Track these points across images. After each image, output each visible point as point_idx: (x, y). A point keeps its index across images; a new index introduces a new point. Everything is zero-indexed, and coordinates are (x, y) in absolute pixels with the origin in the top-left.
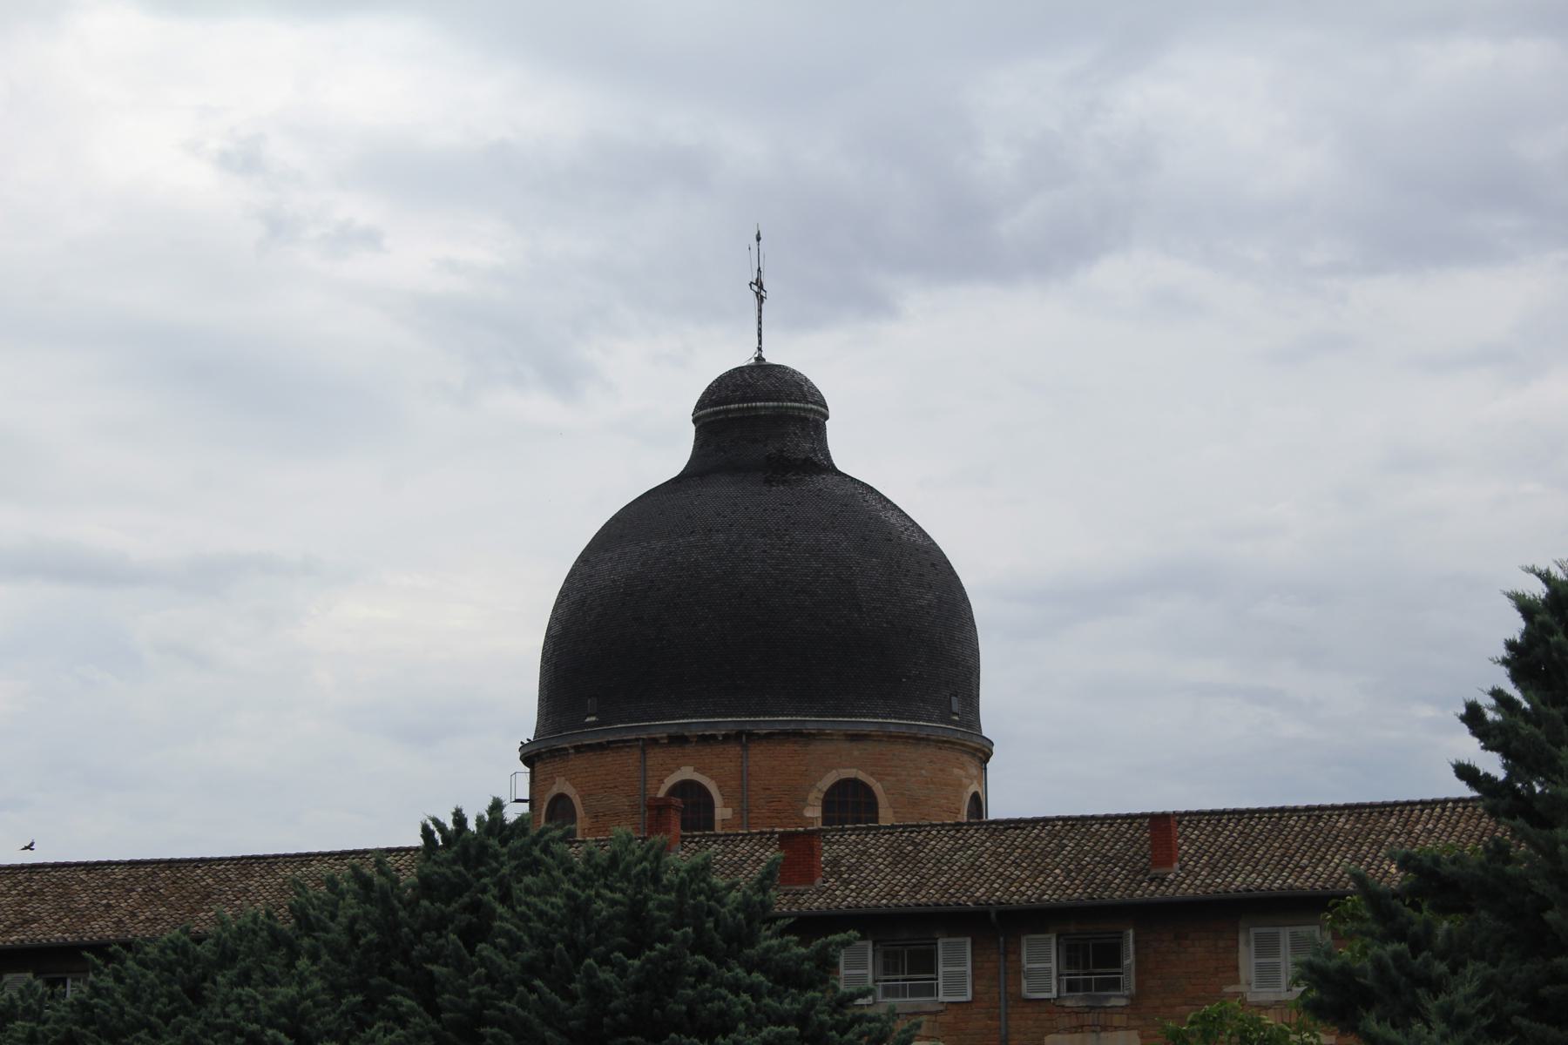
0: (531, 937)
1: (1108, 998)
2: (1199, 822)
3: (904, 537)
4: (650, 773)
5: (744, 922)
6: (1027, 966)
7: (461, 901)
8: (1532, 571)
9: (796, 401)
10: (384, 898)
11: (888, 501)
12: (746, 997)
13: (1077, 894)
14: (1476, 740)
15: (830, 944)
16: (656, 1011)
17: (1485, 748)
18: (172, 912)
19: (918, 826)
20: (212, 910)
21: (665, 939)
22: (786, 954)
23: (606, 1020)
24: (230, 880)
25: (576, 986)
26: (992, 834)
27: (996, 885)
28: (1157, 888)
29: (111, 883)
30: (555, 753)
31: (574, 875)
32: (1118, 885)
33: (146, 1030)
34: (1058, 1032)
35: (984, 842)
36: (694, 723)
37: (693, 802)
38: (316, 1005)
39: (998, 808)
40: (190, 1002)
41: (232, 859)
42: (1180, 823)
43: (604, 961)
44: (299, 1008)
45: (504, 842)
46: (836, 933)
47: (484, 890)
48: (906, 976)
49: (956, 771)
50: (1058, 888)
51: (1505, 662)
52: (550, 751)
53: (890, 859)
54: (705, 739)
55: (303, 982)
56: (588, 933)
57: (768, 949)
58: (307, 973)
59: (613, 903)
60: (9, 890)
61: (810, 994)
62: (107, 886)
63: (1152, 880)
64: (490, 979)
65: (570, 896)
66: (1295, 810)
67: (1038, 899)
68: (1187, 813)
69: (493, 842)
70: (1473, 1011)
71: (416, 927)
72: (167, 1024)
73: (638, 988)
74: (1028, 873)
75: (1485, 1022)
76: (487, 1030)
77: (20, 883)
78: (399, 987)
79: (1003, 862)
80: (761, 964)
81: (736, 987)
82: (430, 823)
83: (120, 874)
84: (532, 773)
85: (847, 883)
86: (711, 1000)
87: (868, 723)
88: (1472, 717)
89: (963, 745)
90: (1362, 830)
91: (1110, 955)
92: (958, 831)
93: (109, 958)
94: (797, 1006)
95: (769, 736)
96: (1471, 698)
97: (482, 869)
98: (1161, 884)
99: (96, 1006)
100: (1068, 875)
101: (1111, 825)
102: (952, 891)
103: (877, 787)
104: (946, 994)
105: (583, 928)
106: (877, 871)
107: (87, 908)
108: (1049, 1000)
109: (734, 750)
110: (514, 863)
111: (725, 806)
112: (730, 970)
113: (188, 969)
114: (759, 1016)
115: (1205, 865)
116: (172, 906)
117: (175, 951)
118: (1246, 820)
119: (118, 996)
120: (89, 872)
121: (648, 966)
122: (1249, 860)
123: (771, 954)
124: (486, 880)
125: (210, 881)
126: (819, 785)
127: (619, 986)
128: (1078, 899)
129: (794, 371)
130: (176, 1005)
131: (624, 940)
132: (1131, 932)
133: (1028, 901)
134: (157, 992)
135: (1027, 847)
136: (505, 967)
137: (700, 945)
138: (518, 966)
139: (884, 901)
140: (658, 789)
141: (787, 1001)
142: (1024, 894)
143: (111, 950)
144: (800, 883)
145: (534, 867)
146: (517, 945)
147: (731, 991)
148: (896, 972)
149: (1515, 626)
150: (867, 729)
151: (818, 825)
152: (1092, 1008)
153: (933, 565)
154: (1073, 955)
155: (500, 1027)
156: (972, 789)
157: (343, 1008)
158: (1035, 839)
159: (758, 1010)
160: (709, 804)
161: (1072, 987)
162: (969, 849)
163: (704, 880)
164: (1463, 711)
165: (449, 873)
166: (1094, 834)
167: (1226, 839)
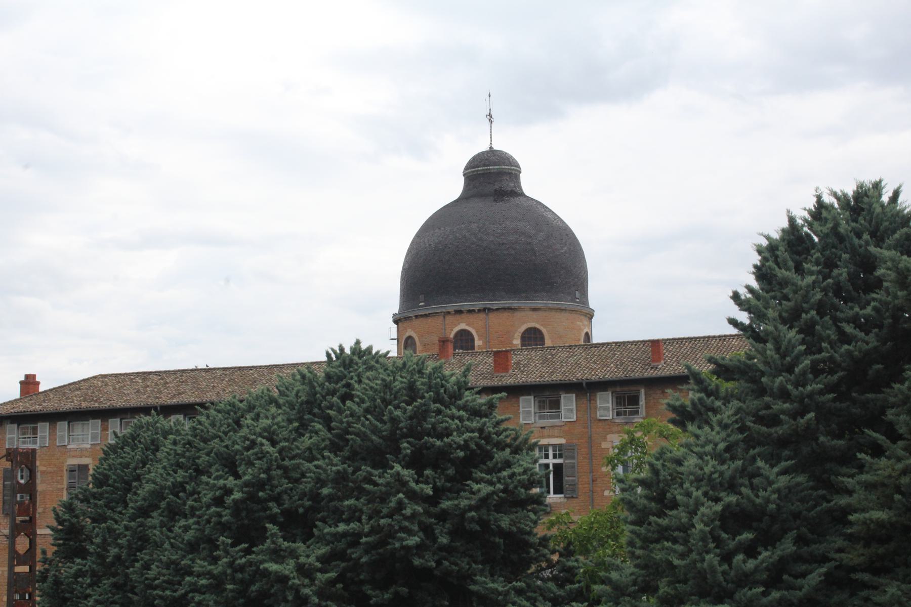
0: (369, 398)
1: (634, 418)
2: (673, 343)
3: (554, 223)
4: (447, 326)
5: (457, 390)
6: (599, 405)
7: (342, 383)
8: (762, 234)
9: (507, 166)
10: (310, 383)
11: (547, 208)
12: (457, 421)
13: (620, 375)
14: (737, 307)
15: (493, 398)
16: (419, 428)
17: (741, 310)
18: (240, 389)
19: (571, 346)
20: (256, 388)
21: (423, 397)
22: (475, 403)
23: (398, 432)
24: (264, 375)
25: (385, 418)
26: (585, 350)
27: (586, 372)
28: (654, 371)
29: (215, 377)
30: (407, 319)
31: (388, 371)
32: (638, 371)
33: (218, 439)
34: (613, 433)
35: (580, 354)
36: (466, 305)
37: (464, 340)
38: (279, 427)
39: (598, 338)
40: (236, 427)
41: (265, 366)
42: (665, 343)
43: (397, 407)
44: (272, 429)
45: (360, 358)
46: (496, 394)
47: (352, 378)
48: (548, 411)
49: (578, 323)
50: (612, 372)
51: (754, 273)
52: (405, 318)
53: (541, 361)
54: (470, 311)
55: (274, 418)
56: (391, 395)
57: (467, 401)
58: (275, 414)
59: (402, 382)
60: (173, 380)
61: (484, 420)
62: (214, 378)
63: (652, 368)
64: (352, 415)
65: (383, 380)
66: (714, 337)
67: (603, 377)
68: (668, 339)
69: (356, 358)
70: (731, 422)
71: (324, 394)
72: (226, 436)
73: (411, 418)
74: (599, 366)
75: (737, 426)
76: (349, 437)
77: (178, 377)
78: (316, 419)
79: (589, 362)
80: (464, 408)
81: (453, 417)
82: (330, 352)
83: (219, 373)
84: (398, 327)
85: (523, 372)
86: (442, 423)
87: (539, 303)
88: (736, 297)
89: (581, 312)
90: (742, 345)
91: (634, 400)
92: (570, 349)
93: (206, 408)
94: (479, 425)
95: (497, 309)
96: (734, 289)
97: (351, 369)
98: (656, 370)
99: (198, 429)
100: (617, 366)
101: (636, 345)
102: (567, 374)
103: (544, 330)
104: (565, 418)
105: (388, 393)
106: (535, 366)
107: (205, 388)
108: (608, 420)
109: (482, 316)
110: (364, 366)
111: (479, 340)
112: (450, 410)
113: (235, 413)
114: (463, 429)
115: (675, 361)
116: (240, 386)
117: (230, 406)
118: (693, 342)
119: (206, 424)
120: (206, 372)
121: (415, 409)
122: (693, 359)
123: (468, 403)
124: (352, 374)
125: (256, 375)
126: (519, 330)
127: (404, 418)
128: (620, 377)
129: (506, 153)
130: (230, 428)
131: (406, 398)
132: (643, 391)
133: (599, 378)
134: (222, 422)
135: (600, 355)
136: (357, 410)
137: (438, 399)
138: (362, 410)
139: (538, 379)
140: (451, 333)
141: (475, 422)
142: (597, 375)
143: (207, 405)
144: (502, 372)
145: (370, 368)
146: (363, 401)
147: (451, 419)
148: (544, 409)
149: (756, 259)
150: (539, 306)
151: (519, 347)
152: (627, 423)
153: (567, 235)
154: (619, 400)
155: (355, 435)
156: (585, 331)
157: (290, 428)
158: (603, 352)
159: (462, 426)
160: (473, 340)
161: (618, 414)
162: (575, 356)
163: (440, 372)
164: (731, 294)
165: (337, 371)
166: (628, 349)
167: (684, 350)
